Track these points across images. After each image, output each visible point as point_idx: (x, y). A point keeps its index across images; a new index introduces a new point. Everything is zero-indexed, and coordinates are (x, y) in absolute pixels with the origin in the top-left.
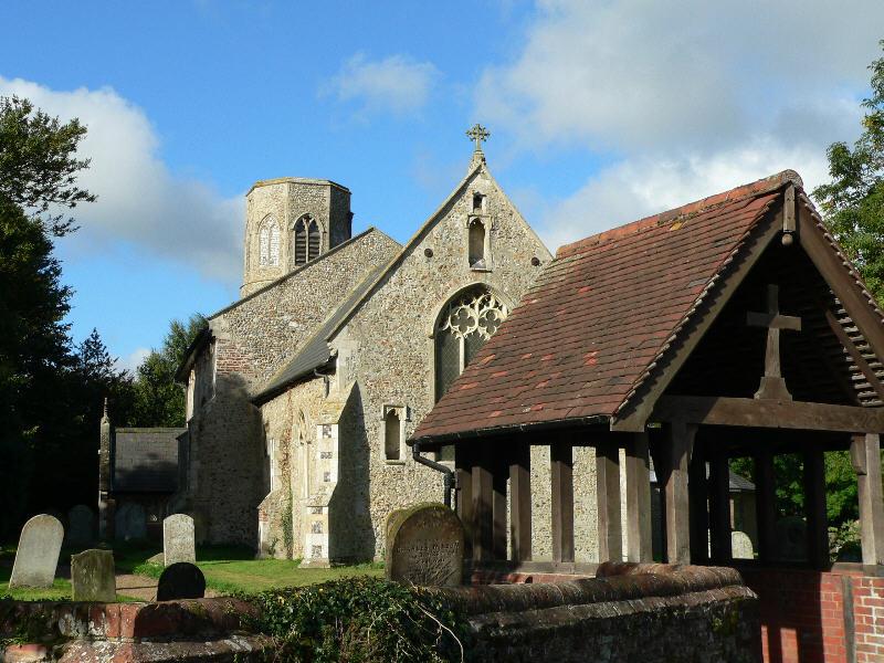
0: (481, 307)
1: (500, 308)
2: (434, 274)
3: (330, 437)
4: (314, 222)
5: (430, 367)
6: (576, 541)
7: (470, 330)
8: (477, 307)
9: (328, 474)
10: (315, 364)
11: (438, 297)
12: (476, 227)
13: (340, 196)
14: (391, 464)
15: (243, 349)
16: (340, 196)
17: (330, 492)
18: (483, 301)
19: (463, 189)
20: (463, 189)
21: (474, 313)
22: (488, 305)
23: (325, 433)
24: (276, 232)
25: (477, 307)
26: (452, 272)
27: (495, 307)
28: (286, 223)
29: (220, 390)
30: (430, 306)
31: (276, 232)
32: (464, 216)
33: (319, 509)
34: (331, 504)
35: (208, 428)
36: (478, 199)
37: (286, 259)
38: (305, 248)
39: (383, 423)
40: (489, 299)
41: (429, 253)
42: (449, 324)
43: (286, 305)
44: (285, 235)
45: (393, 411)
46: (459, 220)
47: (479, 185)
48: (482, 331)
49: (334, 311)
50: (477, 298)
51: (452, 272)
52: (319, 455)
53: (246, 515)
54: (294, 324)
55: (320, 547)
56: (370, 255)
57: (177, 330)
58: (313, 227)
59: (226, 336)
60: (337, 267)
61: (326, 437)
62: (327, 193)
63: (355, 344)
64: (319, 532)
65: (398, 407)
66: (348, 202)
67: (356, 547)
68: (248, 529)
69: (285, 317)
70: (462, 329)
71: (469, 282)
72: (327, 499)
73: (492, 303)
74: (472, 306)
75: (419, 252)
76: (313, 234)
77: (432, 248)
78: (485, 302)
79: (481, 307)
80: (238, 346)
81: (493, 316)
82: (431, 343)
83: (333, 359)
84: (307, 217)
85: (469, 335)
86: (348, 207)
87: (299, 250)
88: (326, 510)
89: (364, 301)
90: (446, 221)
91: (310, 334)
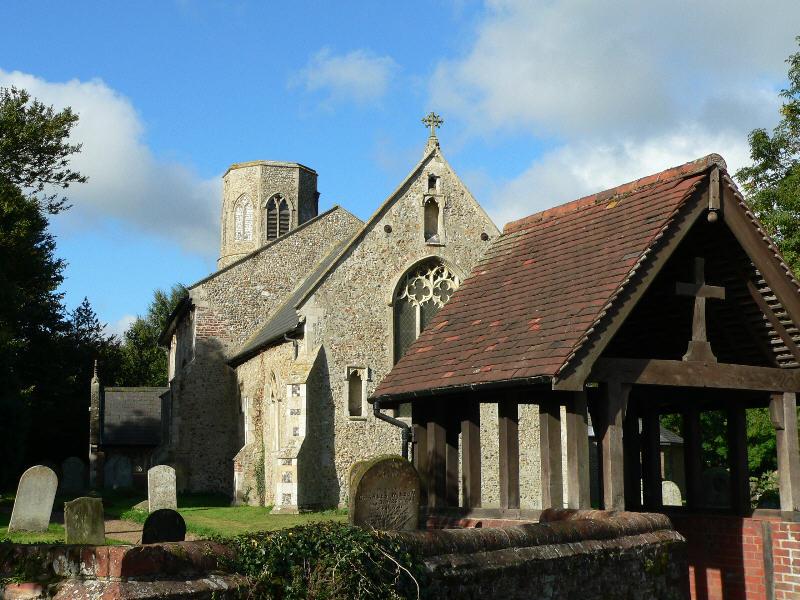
0: (435, 278)
1: (453, 279)
2: (393, 248)
3: (298, 395)
4: (284, 201)
5: (390, 332)
6: (521, 490)
7: (425, 299)
8: (431, 278)
9: (297, 429)
10: (285, 330)
11: (397, 269)
12: (431, 206)
13: (308, 177)
14: (354, 420)
15: (220, 315)
16: (308, 177)
17: (298, 445)
18: (437, 272)
19: (419, 171)
20: (419, 171)
21: (429, 284)
22: (442, 276)
23: (294, 392)
24: (250, 210)
25: (431, 278)
26: (409, 246)
27: (448, 278)
28: (259, 201)
29: (199, 353)
30: (390, 277)
31: (250, 210)
32: (420, 196)
33: (289, 461)
34: (300, 457)
35: (188, 388)
36: (432, 180)
37: (259, 234)
38: (276, 224)
39: (346, 383)
40: (443, 271)
41: (388, 229)
42: (406, 293)
43: (259, 276)
44: (258, 212)
45: (356, 372)
46: (415, 199)
47: (433, 167)
48: (436, 299)
49: (302, 282)
50: (432, 270)
51: (409, 246)
52: (288, 412)
53: (223, 466)
54: (266, 294)
55: (290, 495)
56: (335, 231)
57: (160, 299)
58: (284, 206)
59: (205, 304)
60: (305, 241)
61: (295, 395)
62: (296, 175)
63: (321, 312)
64: (289, 481)
65: (360, 368)
66: (315, 183)
67: (322, 495)
68: (225, 479)
69: (258, 287)
70: (418, 298)
71: (424, 255)
72: (295, 452)
73: (445, 274)
74: (427, 277)
75: (379, 228)
76: (284, 212)
77: (391, 224)
78: (439, 274)
79: (435, 278)
80: (215, 313)
81: (446, 286)
82: (390, 311)
83: (301, 325)
84: (278, 197)
85: (425, 303)
86: (315, 187)
87: (271, 227)
88: (295, 462)
89: (329, 272)
90: (404, 200)
91: (281, 303)
